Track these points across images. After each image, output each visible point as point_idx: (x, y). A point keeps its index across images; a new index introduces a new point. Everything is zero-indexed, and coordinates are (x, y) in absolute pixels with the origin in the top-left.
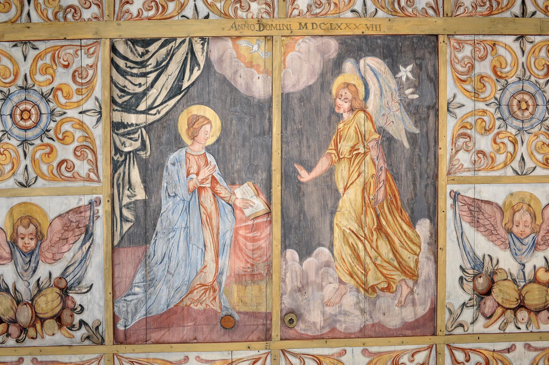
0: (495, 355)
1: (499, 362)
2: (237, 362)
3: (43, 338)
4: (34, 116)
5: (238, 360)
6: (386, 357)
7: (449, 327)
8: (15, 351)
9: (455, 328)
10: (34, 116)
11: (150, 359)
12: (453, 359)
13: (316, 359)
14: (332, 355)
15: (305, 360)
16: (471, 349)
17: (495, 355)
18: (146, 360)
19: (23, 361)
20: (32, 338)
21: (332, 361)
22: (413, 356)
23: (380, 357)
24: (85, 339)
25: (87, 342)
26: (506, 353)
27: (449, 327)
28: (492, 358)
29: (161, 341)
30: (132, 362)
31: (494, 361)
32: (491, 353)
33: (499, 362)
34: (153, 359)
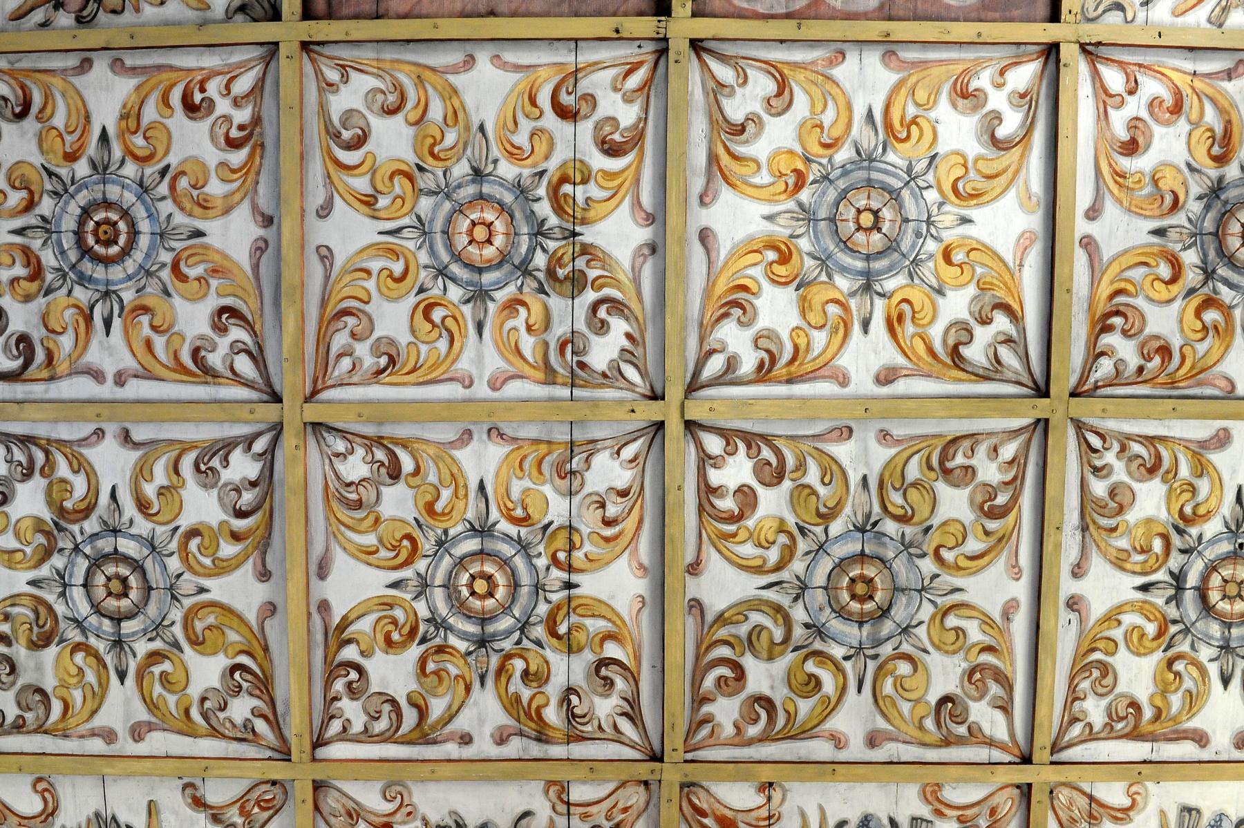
0: (1198, 84)
1: (1204, 98)
2: (589, 69)
3: (137, 10)
4: (110, 215)
5: (590, 65)
6: (936, 71)
7: (1091, 9)
8: (74, 37)
9: (1104, 12)
10: (110, 215)
11: (384, 60)
12: (1098, 85)
13: (773, 70)
14: (812, 63)
15: (749, 71)
16: (1140, 65)
17: (1198, 84)
18: (374, 63)
19: (91, 66)
20: (114, 12)
21: (813, 76)
22: (1002, 73)
23: (926, 72)
24: (235, 12)
25: (239, 17)
26: (1223, 80)
27: (1091, 9)
28: (1189, 91)
29: (416, 12)
30: (343, 67)
31: (1195, 97)
32: (1189, 78)
33: (1204, 98)
34: (392, 61)
